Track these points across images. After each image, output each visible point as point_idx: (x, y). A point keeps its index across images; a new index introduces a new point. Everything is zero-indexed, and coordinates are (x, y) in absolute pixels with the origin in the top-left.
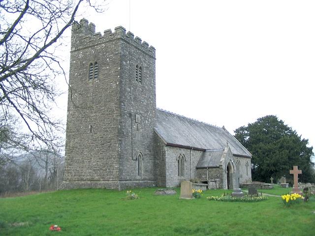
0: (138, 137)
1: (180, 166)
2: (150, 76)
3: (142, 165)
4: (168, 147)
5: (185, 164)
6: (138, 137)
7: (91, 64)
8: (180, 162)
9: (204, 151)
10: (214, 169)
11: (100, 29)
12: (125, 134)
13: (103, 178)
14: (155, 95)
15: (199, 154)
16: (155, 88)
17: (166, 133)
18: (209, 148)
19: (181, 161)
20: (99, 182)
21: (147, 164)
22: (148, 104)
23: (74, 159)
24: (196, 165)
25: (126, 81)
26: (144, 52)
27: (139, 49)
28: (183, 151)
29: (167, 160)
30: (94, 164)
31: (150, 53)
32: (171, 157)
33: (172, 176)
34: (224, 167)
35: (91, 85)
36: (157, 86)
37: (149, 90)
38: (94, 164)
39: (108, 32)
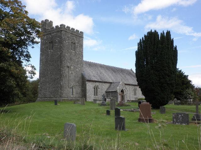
0: (72, 77)
1: (95, 91)
2: (80, 47)
3: (74, 90)
4: (88, 82)
5: (99, 90)
6: (72, 77)
7: (50, 42)
8: (95, 88)
9: (111, 83)
10: (114, 93)
11: (54, 25)
12: (65, 76)
13: (54, 96)
14: (83, 56)
15: (108, 85)
16: (83, 52)
17: (90, 74)
18: (115, 81)
19: (96, 89)
20: (53, 98)
21: (77, 90)
22: (78, 61)
23: (156, 82)
24: (105, 90)
25: (65, 51)
26: (76, 35)
27: (73, 34)
28: (97, 84)
29: (87, 88)
30: (51, 90)
31: (80, 35)
32: (90, 87)
33: (90, 96)
34: (119, 91)
35: (50, 52)
36: (84, 52)
37: (79, 54)
38: (51, 90)
39: (57, 27)
